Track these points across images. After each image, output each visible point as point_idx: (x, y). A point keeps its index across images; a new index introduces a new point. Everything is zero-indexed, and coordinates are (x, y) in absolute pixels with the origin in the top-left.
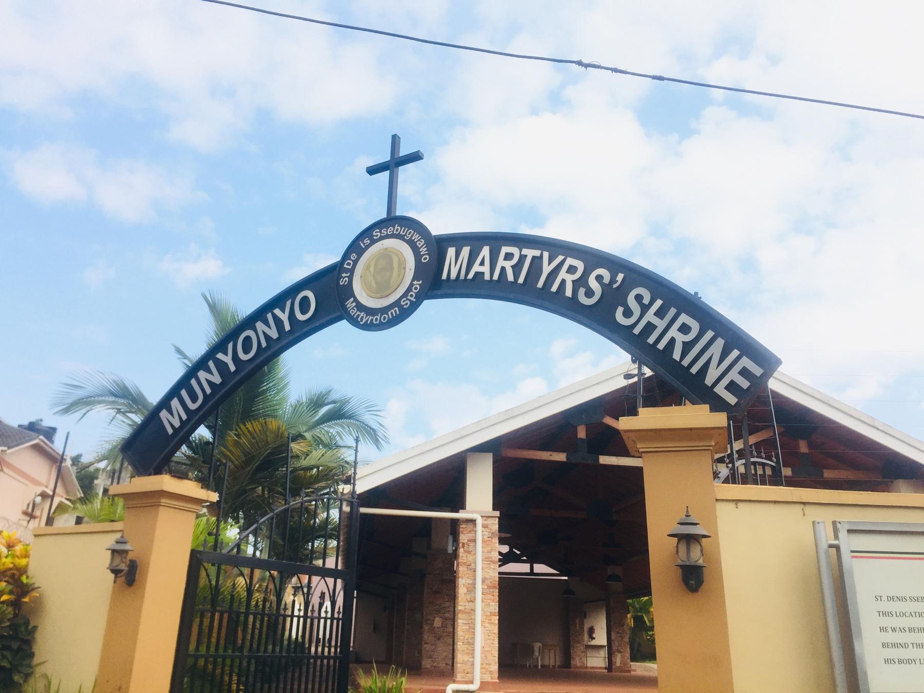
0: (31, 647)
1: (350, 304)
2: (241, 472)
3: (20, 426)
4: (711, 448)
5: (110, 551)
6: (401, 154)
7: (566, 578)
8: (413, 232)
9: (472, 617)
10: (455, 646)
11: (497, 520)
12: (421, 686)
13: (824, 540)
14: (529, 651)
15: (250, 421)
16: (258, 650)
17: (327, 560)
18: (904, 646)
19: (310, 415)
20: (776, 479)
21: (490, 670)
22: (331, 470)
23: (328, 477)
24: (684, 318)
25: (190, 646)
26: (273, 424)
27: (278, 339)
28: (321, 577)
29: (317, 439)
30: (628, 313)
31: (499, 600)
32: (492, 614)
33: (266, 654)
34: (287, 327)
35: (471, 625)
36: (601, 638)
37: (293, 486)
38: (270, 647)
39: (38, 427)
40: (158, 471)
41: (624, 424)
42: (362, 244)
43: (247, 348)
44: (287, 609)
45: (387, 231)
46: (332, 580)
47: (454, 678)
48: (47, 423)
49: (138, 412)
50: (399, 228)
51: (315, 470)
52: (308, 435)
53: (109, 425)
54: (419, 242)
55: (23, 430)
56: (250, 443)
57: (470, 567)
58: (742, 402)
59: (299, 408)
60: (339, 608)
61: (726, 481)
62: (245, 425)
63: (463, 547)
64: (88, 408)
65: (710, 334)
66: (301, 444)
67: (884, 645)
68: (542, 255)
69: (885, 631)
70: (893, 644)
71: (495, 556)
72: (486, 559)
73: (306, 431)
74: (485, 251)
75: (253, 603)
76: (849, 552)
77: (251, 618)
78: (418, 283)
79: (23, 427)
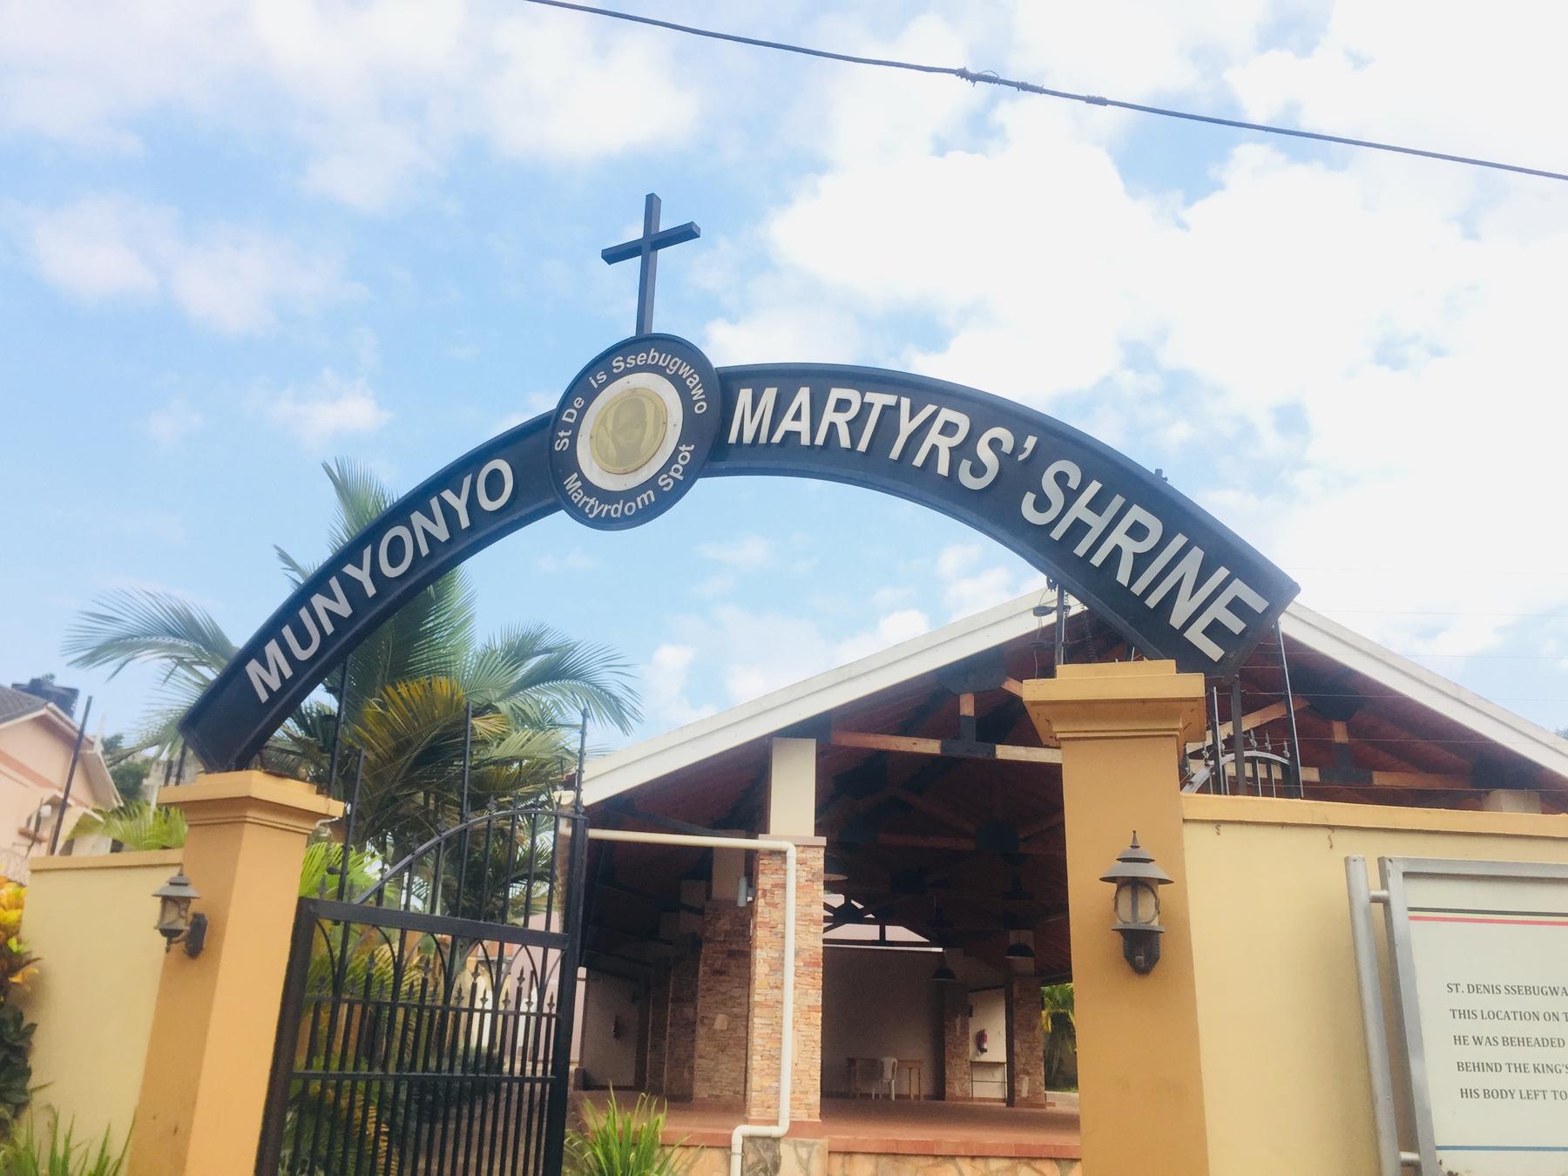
0: (26, 1061)
1: (572, 484)
2: (388, 766)
3: (15, 686)
4: (1178, 733)
5: (159, 899)
6: (662, 228)
7: (940, 950)
8: (679, 362)
9: (778, 1014)
10: (749, 1062)
11: (822, 851)
12: (691, 1129)
13: (1363, 888)
14: (874, 1070)
15: (405, 682)
16: (413, 1067)
17: (532, 919)
18: (1496, 1067)
19: (505, 673)
20: (1289, 787)
21: (806, 1101)
22: (543, 766)
23: (539, 777)
24: (1137, 514)
25: (297, 1058)
26: (443, 686)
27: (448, 541)
28: (520, 946)
29: (520, 712)
30: (1042, 504)
31: (823, 986)
32: (811, 1009)
33: (413, 1074)
34: (465, 522)
35: (777, 1028)
36: (996, 1050)
37: (478, 791)
38: (433, 1063)
39: (48, 688)
40: (242, 764)
41: (1031, 690)
42: (593, 382)
43: (395, 556)
44: (463, 998)
45: (636, 359)
46: (540, 950)
47: (746, 1115)
48: (61, 681)
49: (213, 664)
50: (657, 355)
51: (516, 765)
52: (503, 706)
53: (162, 685)
54: (690, 379)
55: (19, 692)
56: (402, 715)
57: (776, 930)
58: (1231, 656)
59: (489, 659)
60: (552, 997)
61: (1204, 789)
62: (396, 689)
63: (764, 896)
64: (128, 656)
65: (1179, 541)
66: (491, 721)
67: (1461, 1066)
68: (898, 404)
69: (1462, 1042)
70: (1476, 1065)
71: (818, 911)
72: (803, 918)
73: (499, 700)
74: (803, 396)
75: (405, 988)
76: (1406, 910)
77: (400, 1013)
78: (689, 449)
79: (20, 687)
